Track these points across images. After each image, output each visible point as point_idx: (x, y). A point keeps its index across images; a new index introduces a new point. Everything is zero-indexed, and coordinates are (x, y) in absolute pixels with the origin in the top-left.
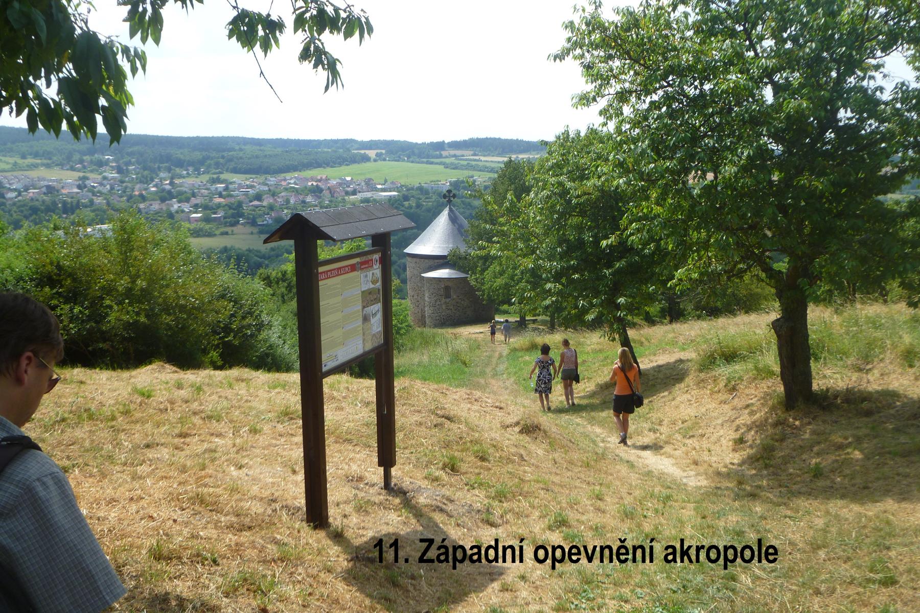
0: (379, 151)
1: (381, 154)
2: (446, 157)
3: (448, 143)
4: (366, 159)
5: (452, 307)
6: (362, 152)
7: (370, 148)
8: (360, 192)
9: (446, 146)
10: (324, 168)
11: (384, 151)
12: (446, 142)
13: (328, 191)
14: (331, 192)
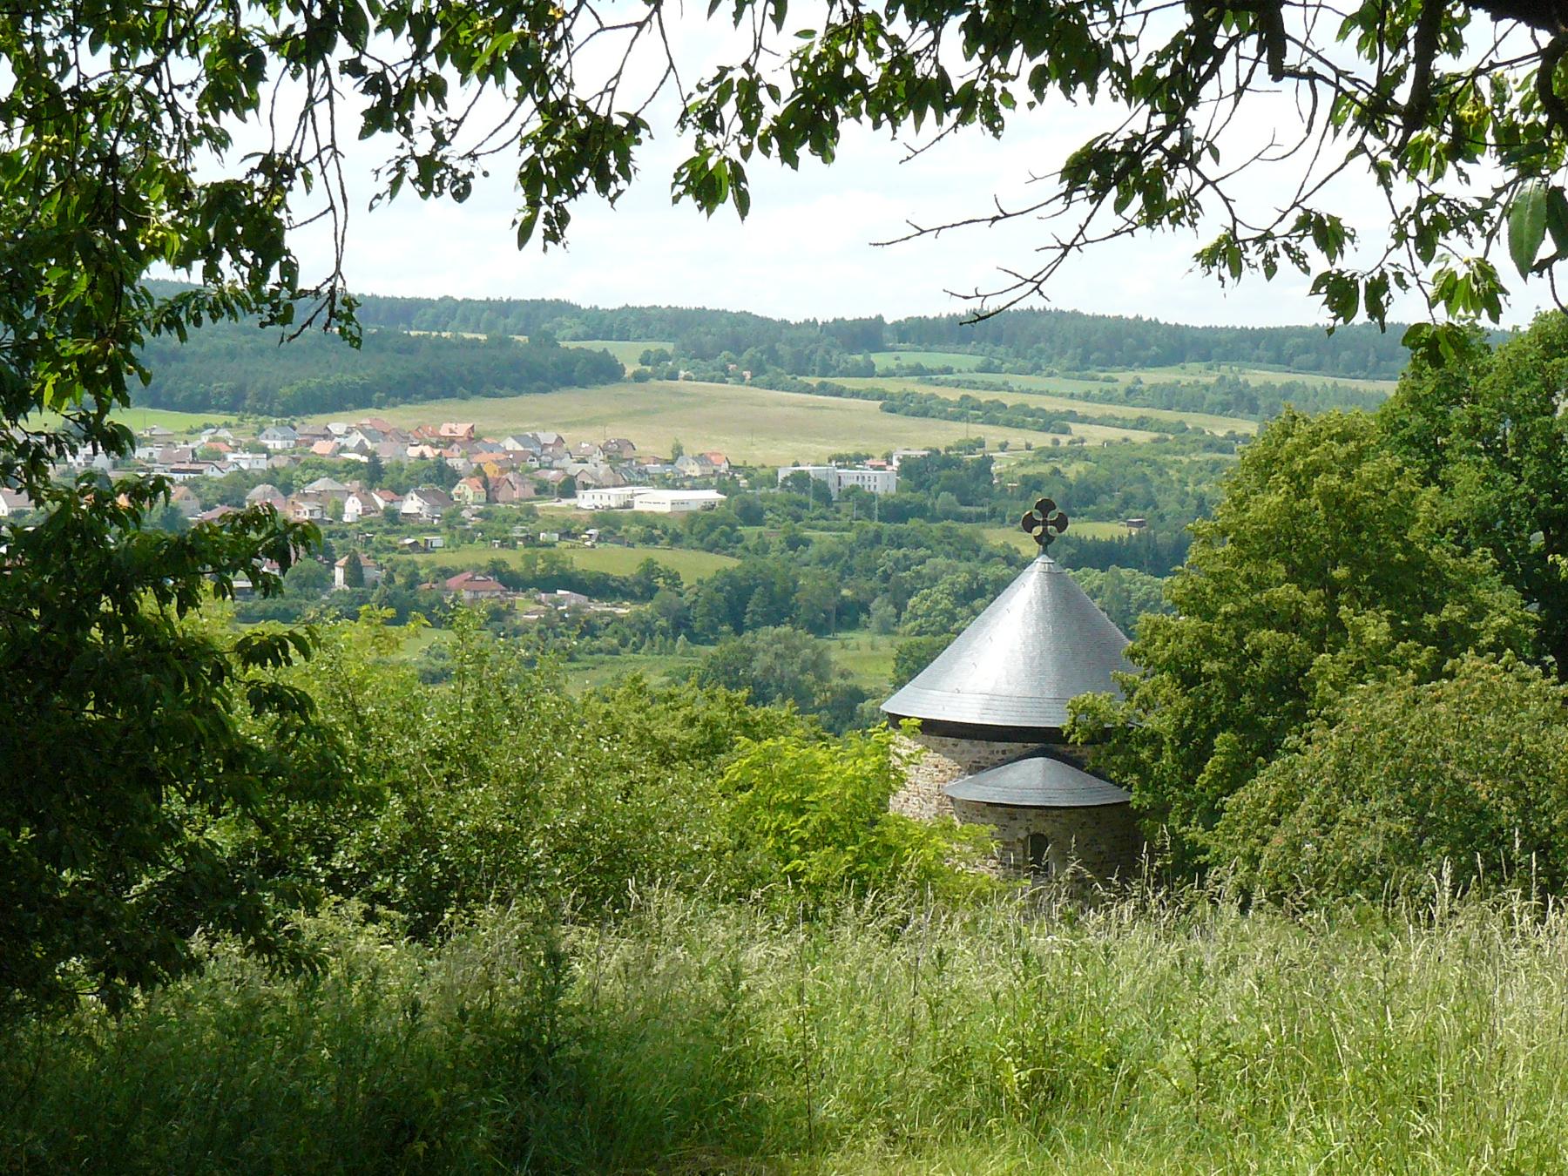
0: (653, 346)
1: (663, 357)
2: (888, 374)
3: (897, 324)
4: (605, 371)
6: (597, 346)
7: (624, 336)
8: (586, 487)
9: (887, 335)
10: (464, 398)
11: (669, 347)
12: (889, 320)
13: (476, 481)
14: (485, 484)
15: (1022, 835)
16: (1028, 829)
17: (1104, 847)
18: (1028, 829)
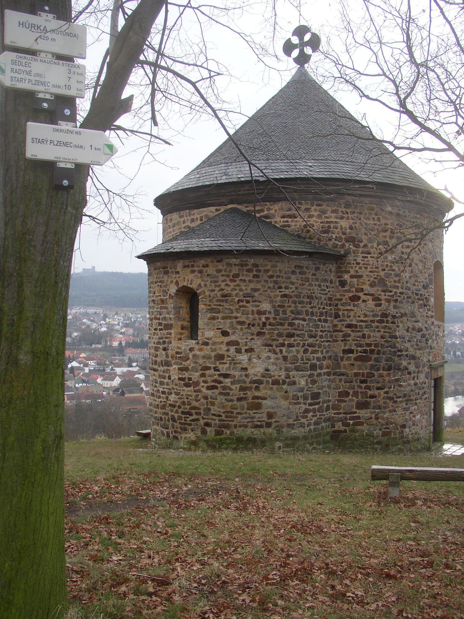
5: (195, 376)
15: (173, 290)
16: (177, 283)
17: (266, 306)
18: (177, 283)
